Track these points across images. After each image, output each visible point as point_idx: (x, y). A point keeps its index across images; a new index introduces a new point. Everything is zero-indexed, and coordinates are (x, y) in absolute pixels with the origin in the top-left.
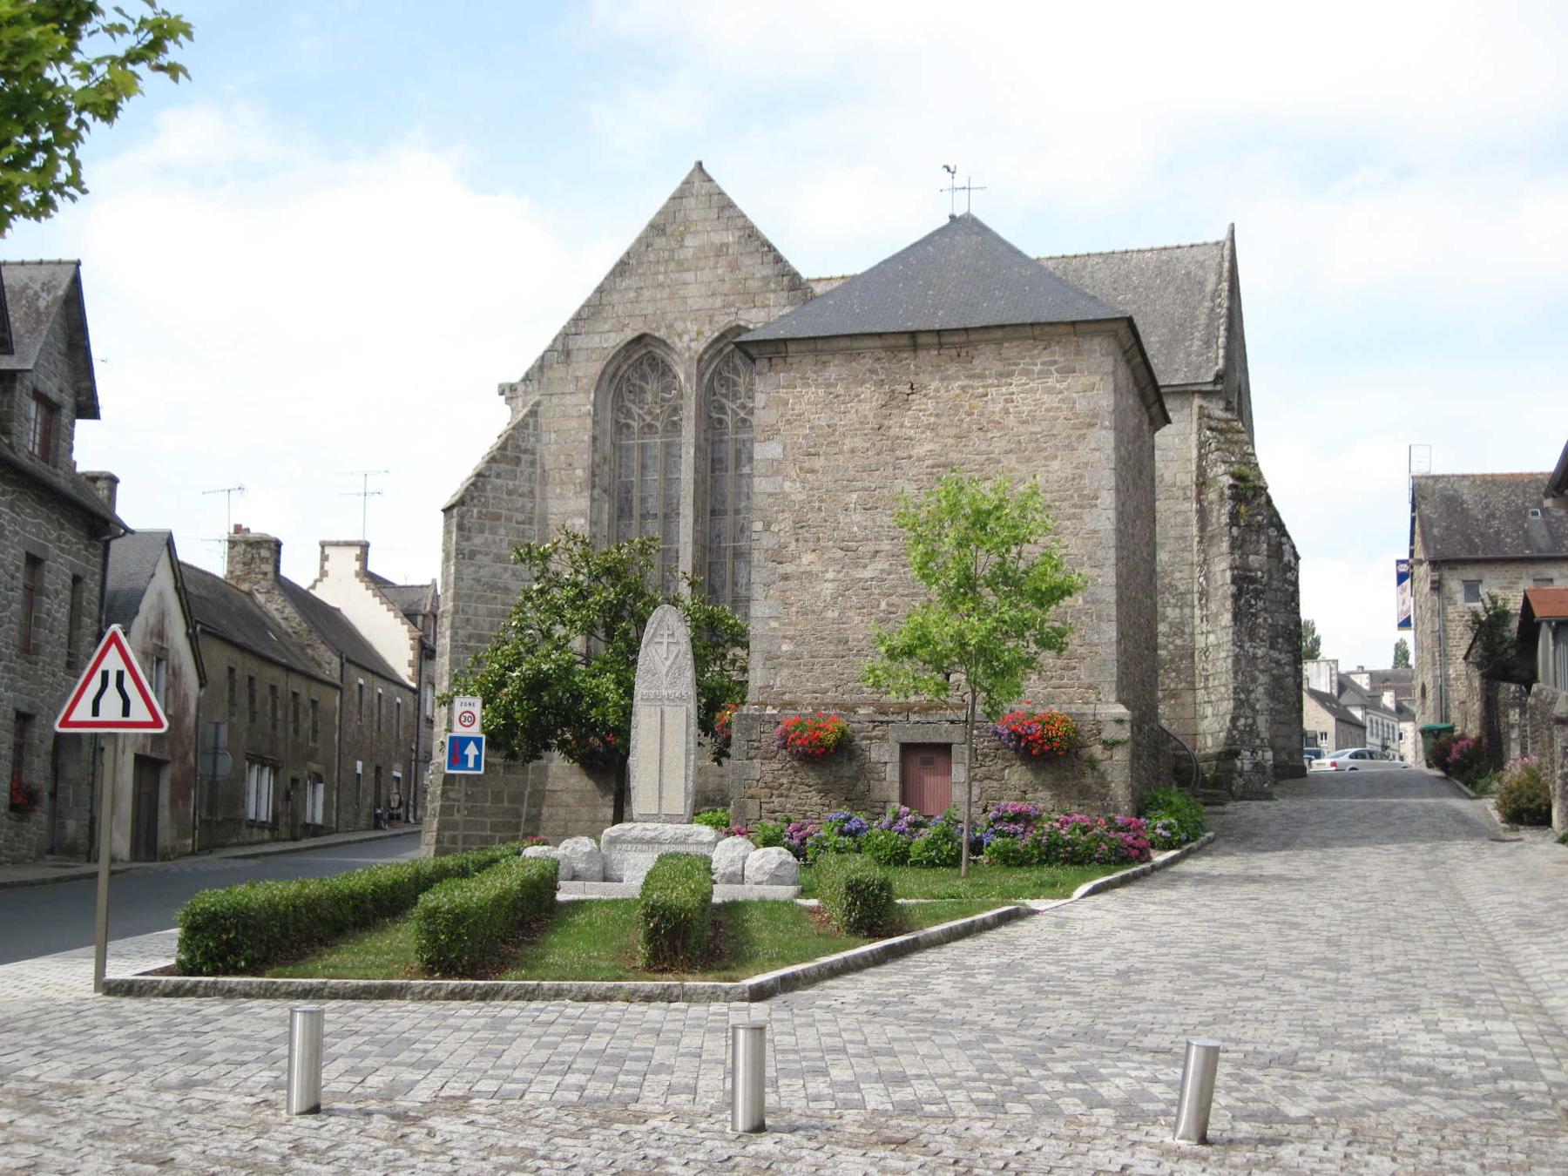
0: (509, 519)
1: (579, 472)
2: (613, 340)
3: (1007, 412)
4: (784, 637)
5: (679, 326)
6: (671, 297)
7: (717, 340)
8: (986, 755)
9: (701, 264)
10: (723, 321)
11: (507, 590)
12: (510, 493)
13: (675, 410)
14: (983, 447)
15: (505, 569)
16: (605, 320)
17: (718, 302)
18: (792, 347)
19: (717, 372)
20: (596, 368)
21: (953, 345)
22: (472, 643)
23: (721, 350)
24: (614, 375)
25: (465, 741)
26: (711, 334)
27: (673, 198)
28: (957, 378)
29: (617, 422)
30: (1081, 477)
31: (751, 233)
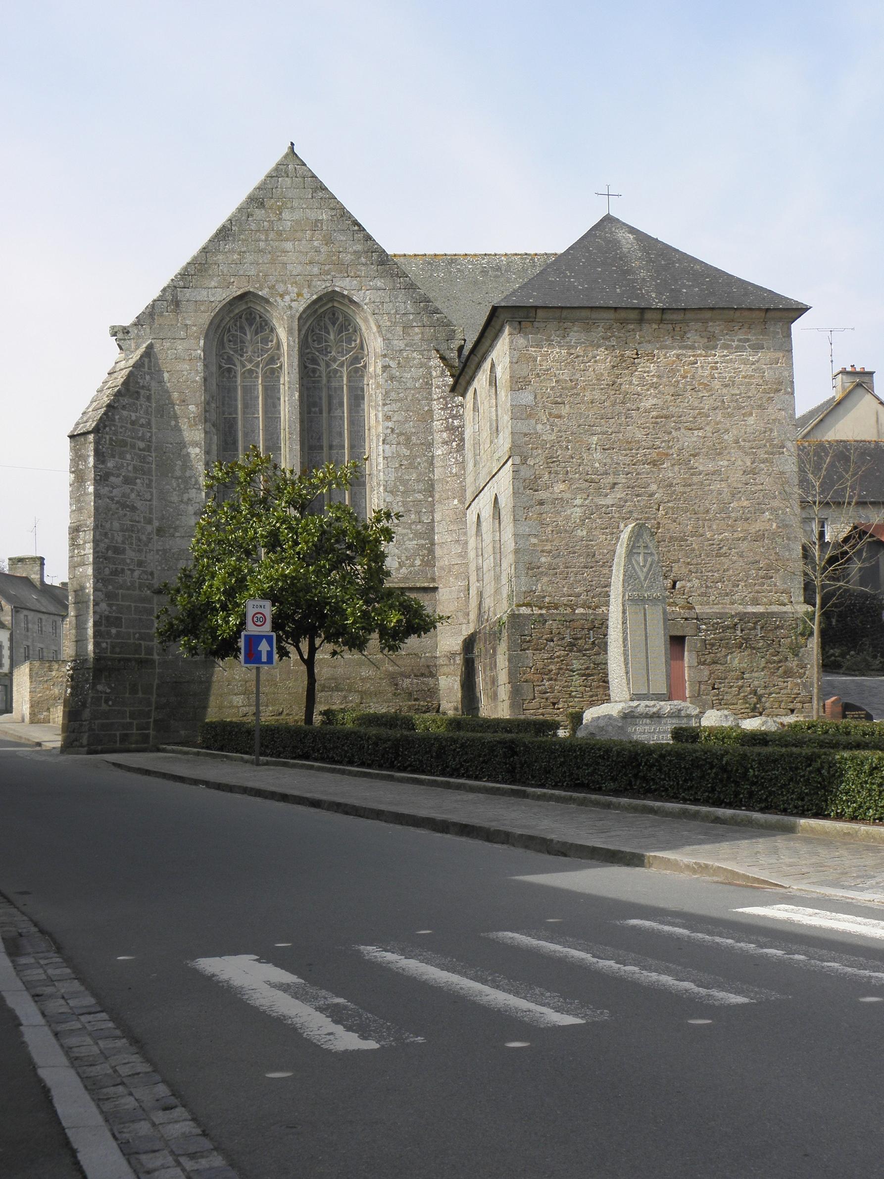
0: (133, 446)
1: (192, 408)
2: (215, 294)
3: (713, 378)
4: (543, 551)
5: (281, 288)
6: (273, 262)
7: (315, 302)
8: (713, 645)
9: (299, 235)
10: (321, 287)
11: (134, 509)
12: (133, 423)
13: (272, 360)
14: (696, 404)
15: (132, 490)
16: (211, 277)
17: (316, 270)
18: (540, 313)
19: (311, 330)
20: (205, 318)
21: (672, 322)
22: (110, 553)
23: (316, 311)
24: (218, 326)
25: (259, 638)
26: (309, 297)
27: (270, 176)
28: (673, 348)
29: (220, 367)
30: (771, 430)
31: (343, 214)
